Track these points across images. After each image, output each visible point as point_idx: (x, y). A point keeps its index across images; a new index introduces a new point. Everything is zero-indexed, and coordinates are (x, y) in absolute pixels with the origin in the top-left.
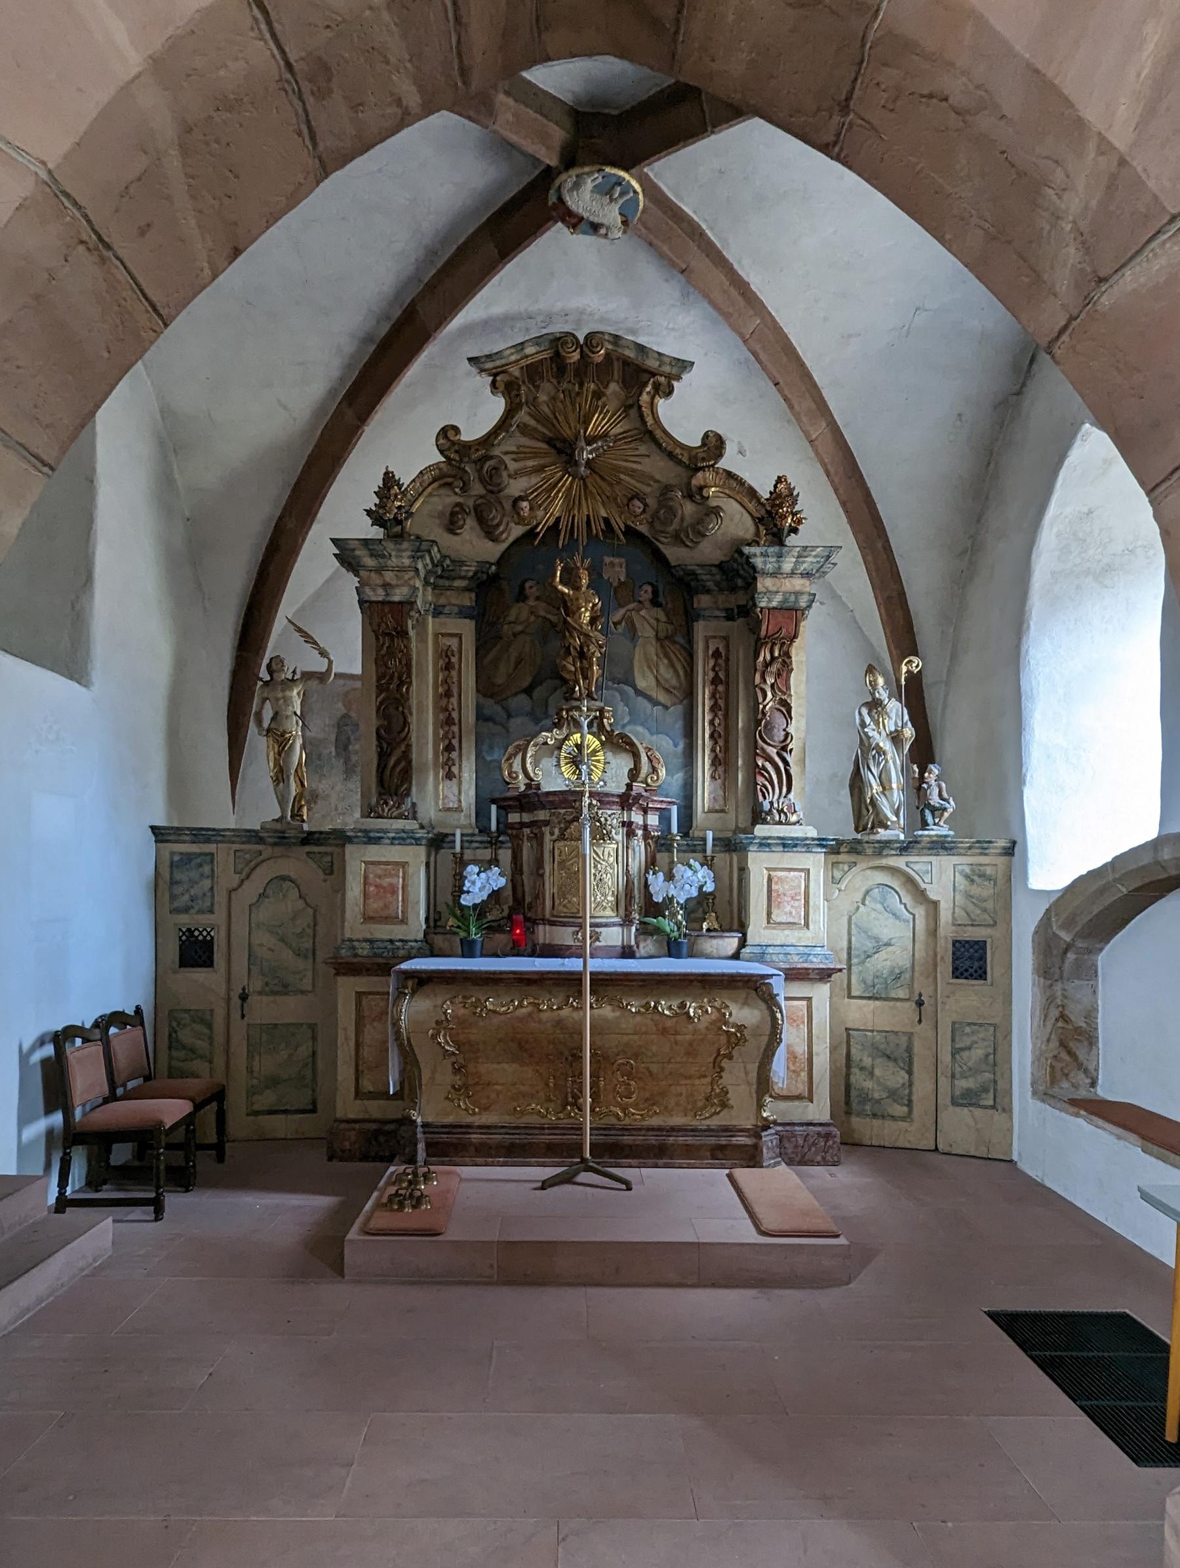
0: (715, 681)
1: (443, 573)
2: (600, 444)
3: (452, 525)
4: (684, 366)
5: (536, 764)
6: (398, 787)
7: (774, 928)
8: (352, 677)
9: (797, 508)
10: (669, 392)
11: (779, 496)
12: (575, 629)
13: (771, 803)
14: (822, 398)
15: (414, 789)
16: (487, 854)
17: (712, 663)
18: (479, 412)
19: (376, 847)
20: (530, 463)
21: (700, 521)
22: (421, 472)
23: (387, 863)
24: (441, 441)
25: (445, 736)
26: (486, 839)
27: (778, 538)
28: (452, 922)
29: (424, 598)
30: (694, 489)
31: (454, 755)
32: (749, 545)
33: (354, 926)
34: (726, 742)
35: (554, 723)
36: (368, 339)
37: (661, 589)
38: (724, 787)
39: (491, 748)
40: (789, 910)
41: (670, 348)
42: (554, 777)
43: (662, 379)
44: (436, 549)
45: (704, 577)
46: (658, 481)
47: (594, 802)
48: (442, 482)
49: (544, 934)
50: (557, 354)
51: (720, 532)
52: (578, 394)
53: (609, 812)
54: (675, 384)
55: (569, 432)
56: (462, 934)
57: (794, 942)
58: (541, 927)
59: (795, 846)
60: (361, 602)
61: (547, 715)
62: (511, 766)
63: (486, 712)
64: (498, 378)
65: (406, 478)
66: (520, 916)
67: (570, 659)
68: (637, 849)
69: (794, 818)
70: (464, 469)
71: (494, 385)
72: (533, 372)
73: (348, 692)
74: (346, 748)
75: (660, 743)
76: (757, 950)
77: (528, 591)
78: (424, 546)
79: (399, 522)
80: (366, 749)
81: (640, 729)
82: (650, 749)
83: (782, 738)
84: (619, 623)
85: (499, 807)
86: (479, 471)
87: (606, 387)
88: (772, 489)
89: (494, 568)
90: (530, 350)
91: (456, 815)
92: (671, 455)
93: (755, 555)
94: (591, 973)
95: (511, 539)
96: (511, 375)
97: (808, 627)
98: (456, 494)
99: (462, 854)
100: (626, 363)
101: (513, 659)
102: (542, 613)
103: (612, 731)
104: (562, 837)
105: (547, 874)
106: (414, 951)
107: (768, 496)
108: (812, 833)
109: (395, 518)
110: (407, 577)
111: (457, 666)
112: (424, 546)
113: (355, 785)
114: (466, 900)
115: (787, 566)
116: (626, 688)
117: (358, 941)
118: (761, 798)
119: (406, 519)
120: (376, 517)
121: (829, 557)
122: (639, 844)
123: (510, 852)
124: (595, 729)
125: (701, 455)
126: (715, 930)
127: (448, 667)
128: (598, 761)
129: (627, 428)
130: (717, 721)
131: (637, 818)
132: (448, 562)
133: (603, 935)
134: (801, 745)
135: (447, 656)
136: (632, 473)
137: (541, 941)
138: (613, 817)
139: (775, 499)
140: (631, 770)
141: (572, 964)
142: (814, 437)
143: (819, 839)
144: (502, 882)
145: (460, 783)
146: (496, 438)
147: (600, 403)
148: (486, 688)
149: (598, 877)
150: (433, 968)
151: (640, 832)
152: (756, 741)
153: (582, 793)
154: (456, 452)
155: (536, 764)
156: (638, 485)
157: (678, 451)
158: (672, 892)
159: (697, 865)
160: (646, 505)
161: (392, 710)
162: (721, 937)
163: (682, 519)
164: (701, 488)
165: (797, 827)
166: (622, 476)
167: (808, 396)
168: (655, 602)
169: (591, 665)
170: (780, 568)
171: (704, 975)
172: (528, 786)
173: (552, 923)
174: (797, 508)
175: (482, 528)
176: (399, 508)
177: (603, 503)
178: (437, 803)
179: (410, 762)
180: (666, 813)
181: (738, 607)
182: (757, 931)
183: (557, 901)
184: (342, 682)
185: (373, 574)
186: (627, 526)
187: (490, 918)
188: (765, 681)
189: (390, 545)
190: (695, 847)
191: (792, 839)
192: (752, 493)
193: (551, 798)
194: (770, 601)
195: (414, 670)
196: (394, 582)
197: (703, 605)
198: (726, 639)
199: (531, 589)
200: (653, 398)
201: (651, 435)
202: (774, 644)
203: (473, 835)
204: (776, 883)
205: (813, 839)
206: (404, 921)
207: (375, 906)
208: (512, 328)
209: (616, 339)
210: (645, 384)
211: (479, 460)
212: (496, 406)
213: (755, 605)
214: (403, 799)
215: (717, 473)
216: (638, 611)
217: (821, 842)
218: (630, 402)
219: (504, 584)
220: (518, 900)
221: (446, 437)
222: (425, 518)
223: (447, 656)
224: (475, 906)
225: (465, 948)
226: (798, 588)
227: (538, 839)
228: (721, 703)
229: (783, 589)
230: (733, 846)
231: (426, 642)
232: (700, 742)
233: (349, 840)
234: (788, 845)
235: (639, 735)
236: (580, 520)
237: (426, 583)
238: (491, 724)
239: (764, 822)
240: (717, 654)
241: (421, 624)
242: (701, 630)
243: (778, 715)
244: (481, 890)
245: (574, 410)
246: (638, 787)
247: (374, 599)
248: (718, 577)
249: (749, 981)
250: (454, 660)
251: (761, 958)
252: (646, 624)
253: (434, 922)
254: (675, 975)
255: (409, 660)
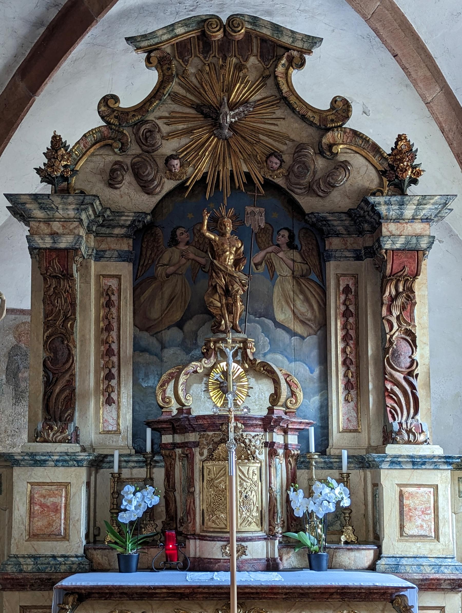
0: (346, 314)
1: (104, 223)
2: (241, 109)
3: (112, 181)
4: (314, 41)
5: (187, 391)
6: (63, 412)
7: (407, 541)
8: (22, 312)
9: (416, 162)
10: (301, 64)
11: (400, 152)
12: (221, 270)
13: (400, 424)
14: (436, 67)
15: (77, 414)
16: (142, 473)
17: (343, 297)
18: (135, 83)
19: (41, 469)
20: (181, 126)
21: (330, 174)
22: (85, 135)
23: (52, 484)
24: (103, 108)
25: (106, 366)
26: (141, 458)
27: (399, 188)
28: (110, 537)
29: (87, 244)
30: (324, 147)
31: (114, 383)
32: (374, 194)
33: (20, 544)
34: (358, 367)
35: (203, 353)
36: (38, 24)
37: (296, 232)
38: (357, 410)
39: (147, 375)
40: (419, 524)
41: (302, 26)
42: (202, 402)
43: (295, 53)
44: (98, 202)
45: (335, 223)
46: (293, 141)
47: (239, 425)
48: (102, 143)
49: (194, 548)
50: (203, 33)
51: (349, 182)
52: (222, 67)
53: (253, 434)
54: (307, 57)
55: (215, 100)
56: (120, 550)
57: (426, 553)
58: (192, 542)
59: (424, 463)
60: (31, 249)
61: (196, 345)
62: (164, 391)
63: (143, 343)
64: (152, 54)
65: (71, 139)
66: (172, 532)
67: (217, 297)
68: (279, 466)
69: (421, 438)
70: (122, 132)
71: (148, 60)
72: (182, 49)
73: (18, 326)
74: (15, 375)
75: (298, 370)
76: (392, 562)
77: (179, 238)
78: (88, 200)
79: (65, 179)
80: (33, 378)
81: (279, 357)
82: (289, 376)
83: (408, 364)
84: (260, 264)
85: (153, 429)
86: (136, 134)
87: (247, 60)
88: (393, 146)
89: (149, 217)
90: (180, 30)
91: (115, 437)
92: (303, 118)
93: (379, 204)
94: (238, 587)
95: (164, 192)
96: (163, 52)
97: (428, 265)
98: (116, 153)
99: (120, 474)
100: (264, 40)
101: (166, 296)
102: (191, 256)
103: (255, 360)
104: (210, 457)
105: (197, 491)
106: (75, 566)
107: (389, 152)
108: (438, 451)
109: (62, 176)
110: (72, 227)
111: (116, 303)
112: (88, 200)
113: (23, 409)
114: (124, 518)
115: (409, 212)
116: (268, 321)
117: (24, 557)
118: (391, 420)
119: (72, 176)
120: (45, 175)
121: (446, 204)
122: (280, 463)
123: (163, 471)
124: (239, 358)
125: (330, 117)
126: (352, 543)
127: (109, 304)
128: (243, 386)
129: (264, 95)
130: (348, 350)
131: (278, 438)
132: (108, 212)
133: (249, 548)
134: (425, 370)
135: (107, 294)
136: (270, 134)
137: (192, 555)
138: (256, 438)
139: (396, 155)
140: (272, 395)
141: (220, 578)
142: (430, 99)
143: (446, 457)
144: (156, 500)
145: (119, 408)
146: (150, 105)
147: (241, 74)
148: (142, 323)
149: (244, 494)
150: (92, 584)
151: (281, 451)
152: (384, 368)
153: (226, 419)
154: (116, 117)
155: (187, 391)
156: (276, 144)
157: (310, 114)
158: (312, 508)
159: (334, 482)
160: (282, 161)
161: (57, 343)
162: (358, 549)
163: (315, 173)
164: (330, 146)
165: (425, 446)
166: (261, 137)
167: (423, 65)
168: (291, 245)
169: (235, 302)
170: (402, 214)
171: (344, 588)
172: (180, 411)
173: (202, 538)
174: (416, 162)
175: (138, 183)
176: (65, 166)
177: (244, 160)
178: (97, 426)
179: (73, 390)
180: (304, 433)
181: (366, 248)
182: (392, 544)
183: (206, 518)
184: (13, 316)
185: (42, 224)
186: (266, 180)
187: (145, 533)
188: (391, 314)
189: (57, 200)
190: (332, 464)
191: (420, 457)
192: (376, 149)
193: (201, 422)
194: (394, 243)
195: (78, 308)
196: (60, 231)
197: (334, 247)
198: (355, 277)
199: (183, 235)
200: (287, 69)
201: (287, 101)
202: (398, 281)
203: (130, 455)
204: (408, 498)
205: (440, 457)
206: (66, 538)
207: (40, 524)
208: (165, 11)
209: (255, 20)
210: (280, 58)
211: (136, 124)
212: (152, 78)
213: (380, 247)
214: (67, 425)
215: (345, 132)
216: (276, 253)
217: (447, 460)
218: (267, 73)
219: (159, 231)
220: (171, 516)
221: (107, 105)
222: (88, 174)
223: (107, 294)
224: (131, 523)
225: (122, 562)
226: (418, 231)
227: (189, 458)
228: (352, 333)
229: (405, 232)
230: (364, 462)
231: (89, 283)
232: (334, 368)
233: (17, 463)
234: (417, 463)
235: (279, 363)
236: (224, 175)
237: (89, 231)
238: (147, 355)
239: (394, 441)
240: (347, 290)
241: (85, 268)
242: (332, 268)
243: (404, 344)
244: (137, 508)
245: (218, 80)
246: (279, 411)
247: (42, 246)
248: (347, 223)
249: (384, 593)
250: (114, 298)
251: (395, 570)
252: (284, 266)
253: (93, 538)
254: (316, 588)
255: (74, 299)
